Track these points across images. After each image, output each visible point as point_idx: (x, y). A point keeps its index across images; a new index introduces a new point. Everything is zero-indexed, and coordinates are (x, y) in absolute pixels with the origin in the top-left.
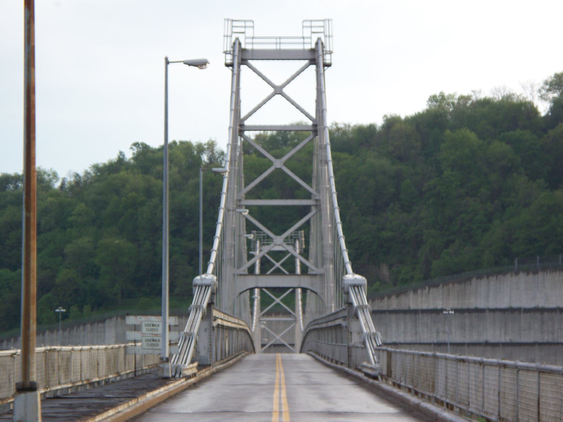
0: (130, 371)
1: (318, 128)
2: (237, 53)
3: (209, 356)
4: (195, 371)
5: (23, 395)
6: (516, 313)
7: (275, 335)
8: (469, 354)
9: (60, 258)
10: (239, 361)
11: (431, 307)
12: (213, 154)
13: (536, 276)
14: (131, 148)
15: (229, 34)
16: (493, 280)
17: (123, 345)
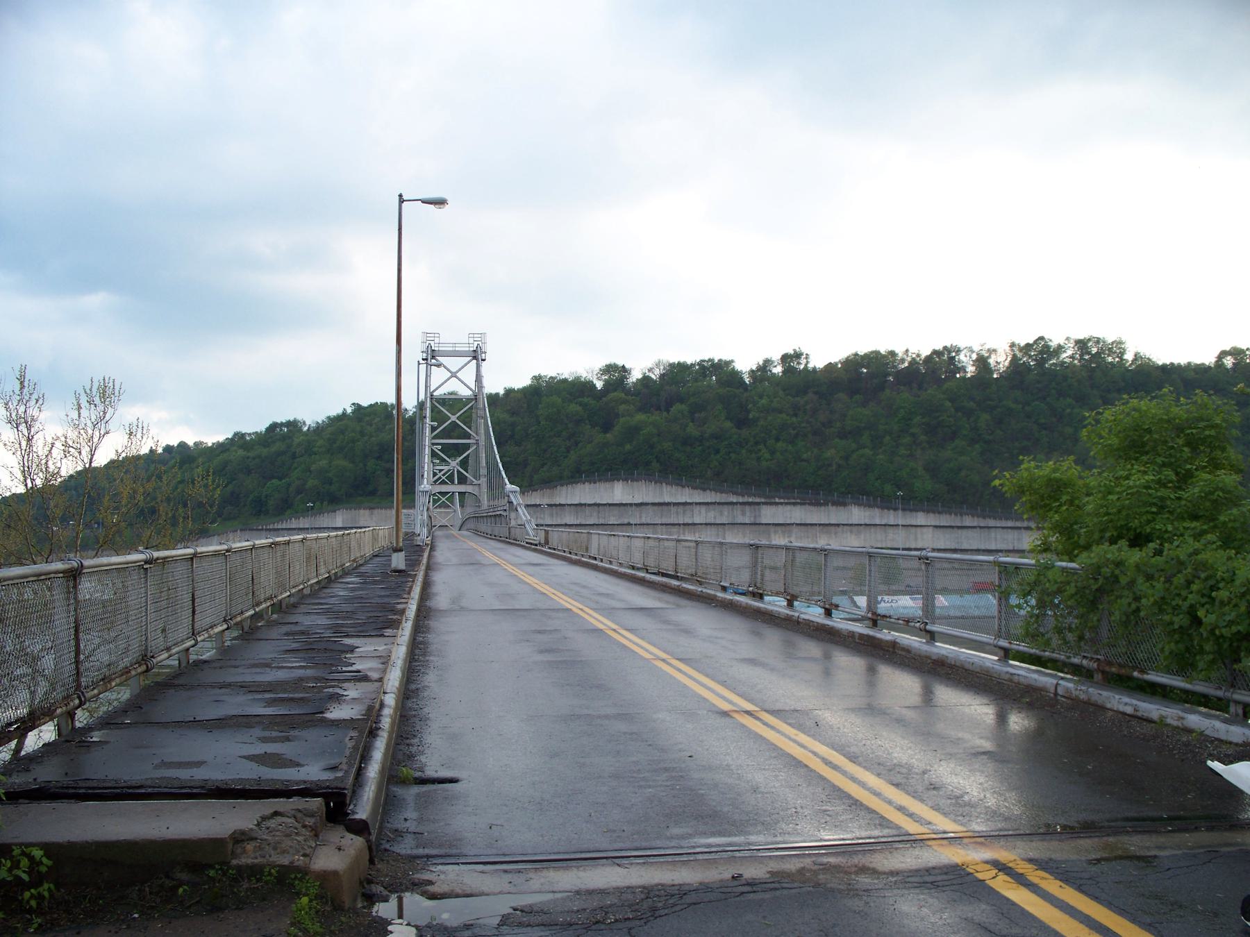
8: (207, 545)
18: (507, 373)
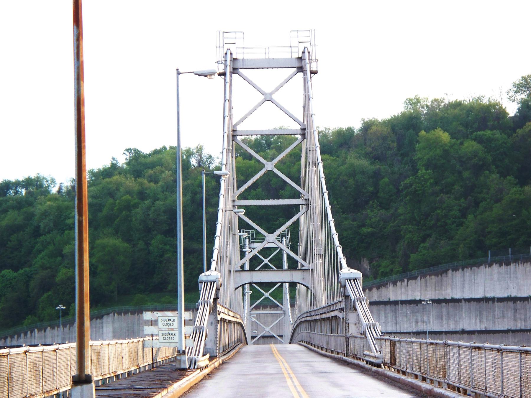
0: (147, 364)
1: (306, 131)
2: (228, 62)
3: (215, 348)
4: (207, 362)
5: (79, 387)
6: (491, 302)
7: (265, 327)
9: (59, 258)
10: (238, 352)
11: (410, 298)
12: (201, 157)
13: (509, 267)
14: (124, 153)
15: (221, 45)
16: (468, 272)
17: (141, 339)
18: (359, 96)
